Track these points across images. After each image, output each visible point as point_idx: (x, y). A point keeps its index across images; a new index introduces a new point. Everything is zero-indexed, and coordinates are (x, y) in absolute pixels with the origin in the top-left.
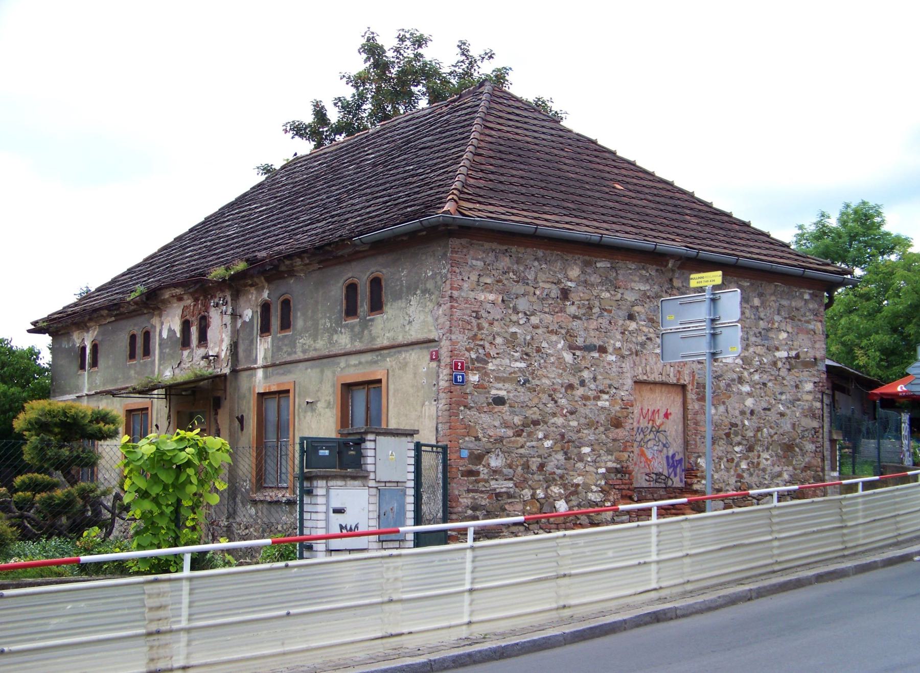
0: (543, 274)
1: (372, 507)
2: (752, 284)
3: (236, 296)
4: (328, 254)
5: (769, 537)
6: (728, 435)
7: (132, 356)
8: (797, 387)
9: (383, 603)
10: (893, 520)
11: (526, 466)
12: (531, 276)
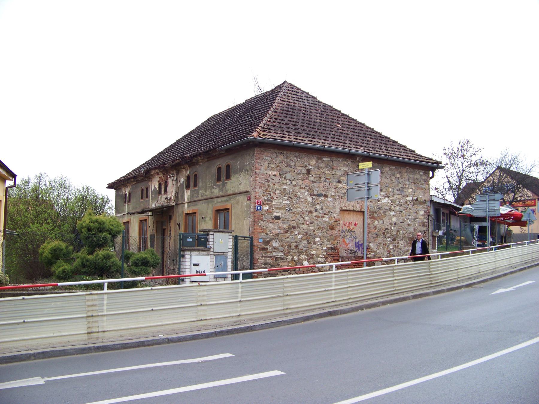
0: (299, 163)
1: (211, 263)
2: (396, 168)
3: (178, 173)
4: (210, 155)
5: (393, 279)
6: (384, 233)
7: (142, 198)
8: (416, 213)
9: (197, 306)
10: (456, 271)
11: (289, 246)
12: (293, 164)
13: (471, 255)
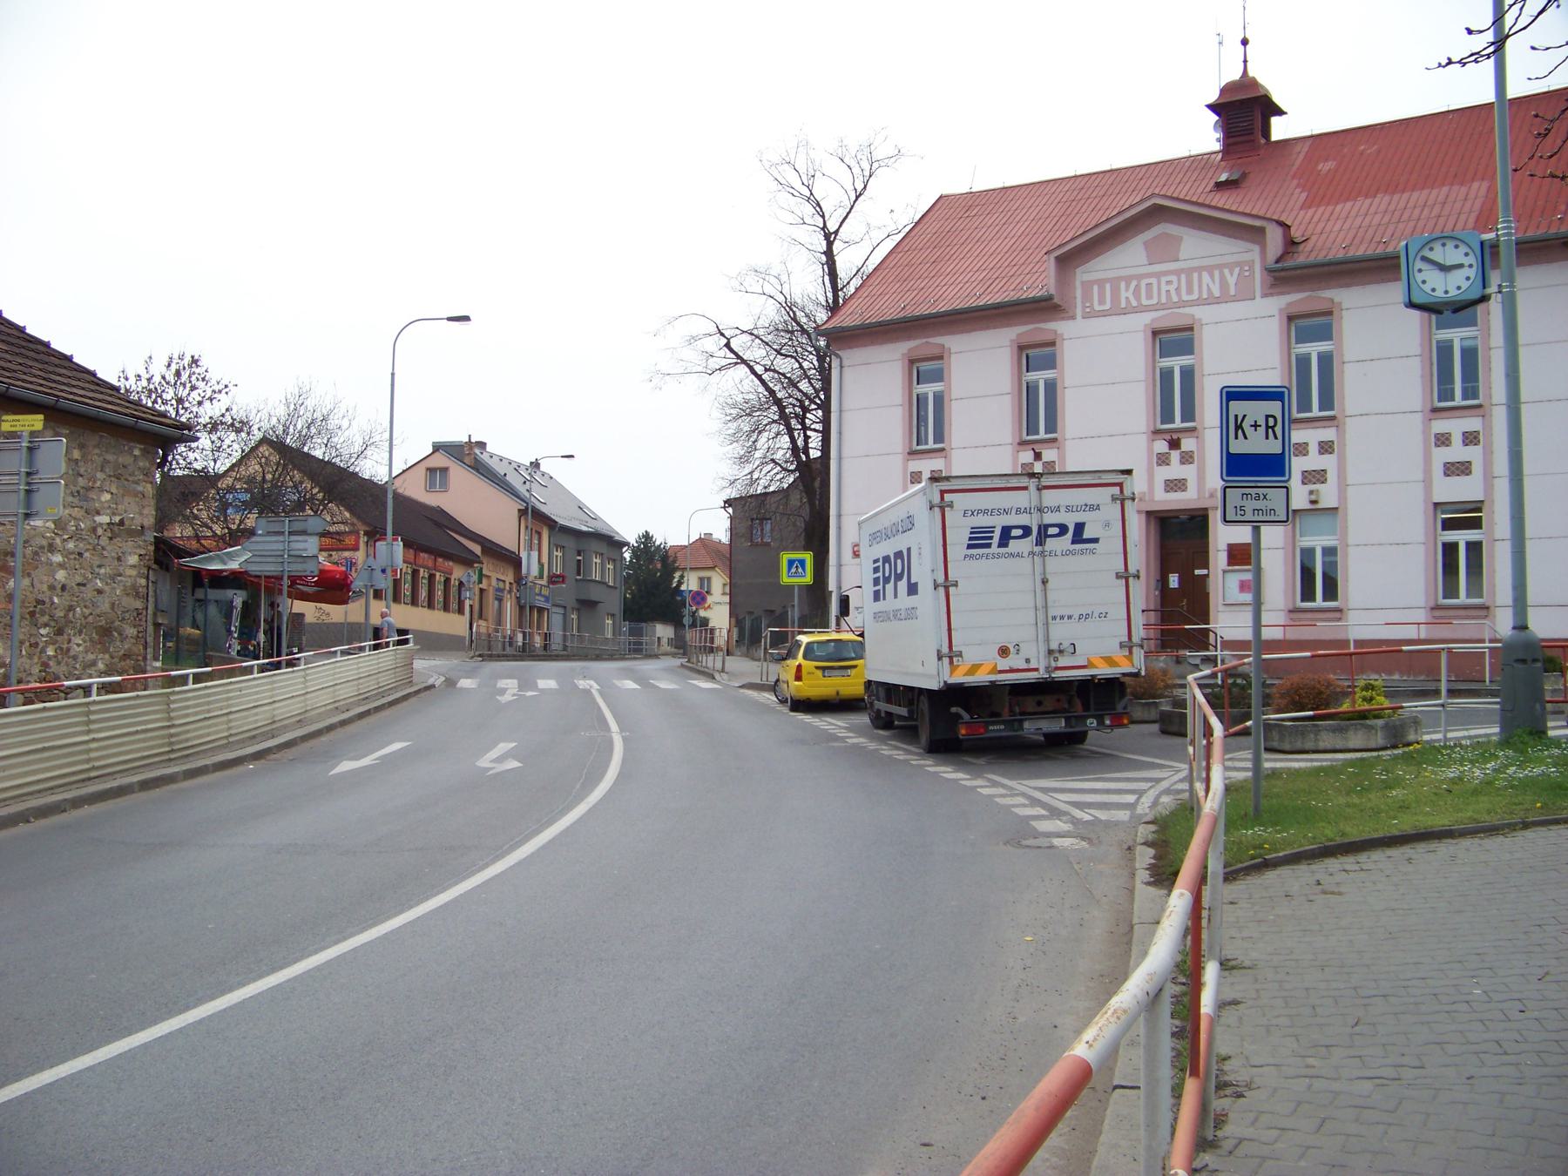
5: (86, 738)
6: (32, 614)
8: (119, 559)
13: (191, 686)
